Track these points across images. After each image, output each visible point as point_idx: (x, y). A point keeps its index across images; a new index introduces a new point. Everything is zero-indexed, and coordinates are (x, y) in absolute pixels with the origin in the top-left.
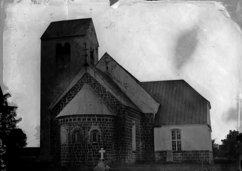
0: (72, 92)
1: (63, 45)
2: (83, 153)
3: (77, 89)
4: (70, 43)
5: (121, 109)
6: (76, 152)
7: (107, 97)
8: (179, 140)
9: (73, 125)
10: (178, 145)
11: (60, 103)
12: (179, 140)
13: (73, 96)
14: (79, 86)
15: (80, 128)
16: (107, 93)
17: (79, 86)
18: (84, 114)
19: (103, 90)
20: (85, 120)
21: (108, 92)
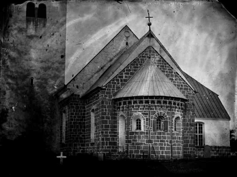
0: (131, 67)
1: (37, 6)
2: (167, 144)
3: (137, 65)
4: (47, 6)
5: (189, 95)
6: (160, 142)
7: (174, 78)
8: (201, 134)
9: (155, 109)
10: (199, 139)
11: (115, 79)
12: (201, 134)
13: (131, 71)
14: (140, 61)
15: (164, 113)
16: (173, 74)
17: (140, 61)
18: (146, 94)
19: (168, 70)
20: (154, 104)
21: (174, 73)
